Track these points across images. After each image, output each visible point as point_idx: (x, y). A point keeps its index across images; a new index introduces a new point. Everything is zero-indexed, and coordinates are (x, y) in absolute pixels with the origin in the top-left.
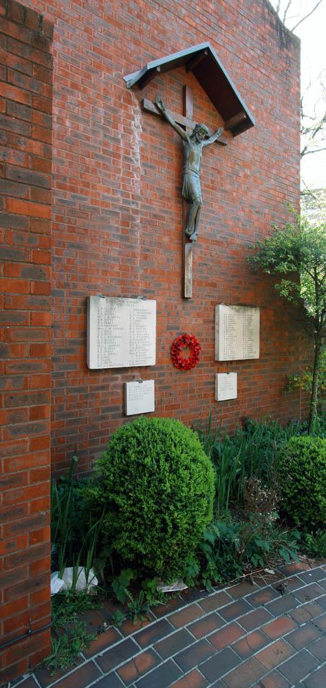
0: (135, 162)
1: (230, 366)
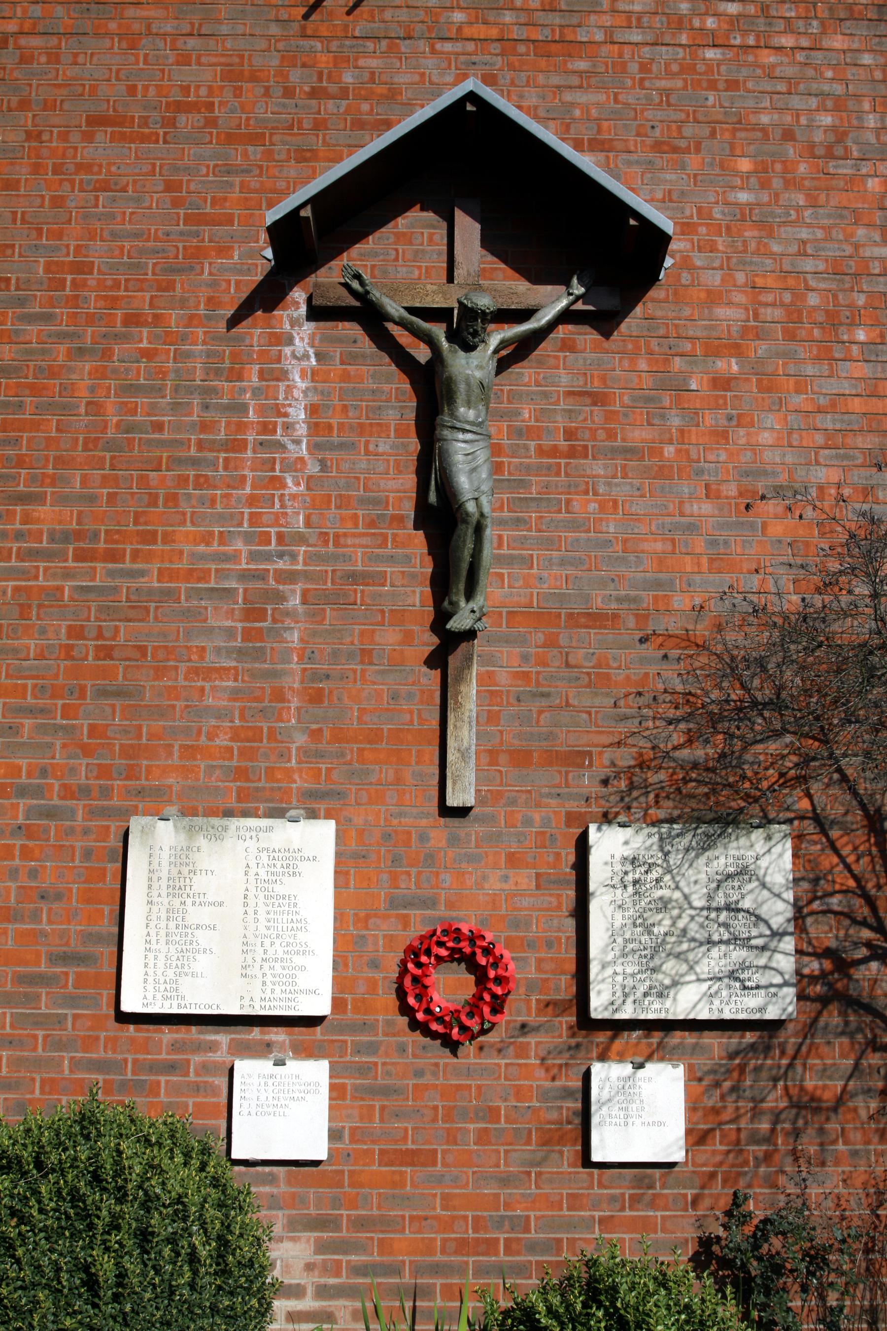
0: (291, 446)
1: (657, 1036)
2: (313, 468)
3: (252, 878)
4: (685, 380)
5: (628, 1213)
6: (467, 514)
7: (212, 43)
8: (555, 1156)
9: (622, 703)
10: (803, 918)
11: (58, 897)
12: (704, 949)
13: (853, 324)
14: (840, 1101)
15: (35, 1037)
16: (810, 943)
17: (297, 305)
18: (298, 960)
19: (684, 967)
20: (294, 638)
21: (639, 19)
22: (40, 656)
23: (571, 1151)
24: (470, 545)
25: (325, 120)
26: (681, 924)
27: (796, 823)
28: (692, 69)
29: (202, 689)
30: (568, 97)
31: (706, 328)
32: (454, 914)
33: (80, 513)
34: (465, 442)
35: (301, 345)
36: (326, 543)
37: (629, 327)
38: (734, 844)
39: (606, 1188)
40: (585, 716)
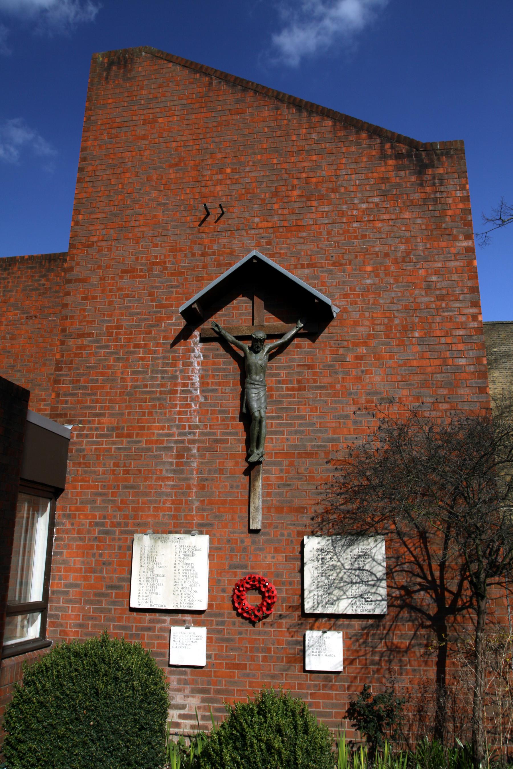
0: (194, 392)
2: (202, 400)
3: (177, 557)
4: (345, 357)
5: (321, 691)
6: (255, 417)
7: (166, 238)
8: (293, 668)
9: (319, 487)
10: (393, 573)
11: (109, 564)
12: (349, 585)
13: (413, 330)
14: (408, 649)
15: (101, 616)
16: (395, 583)
17: (196, 337)
18: (194, 588)
19: (342, 593)
20: (195, 465)
21: (327, 214)
22: (104, 474)
23: (298, 666)
24: (257, 428)
25: (207, 264)
26: (340, 575)
27: (389, 534)
28: (348, 232)
29: (161, 485)
30: (299, 247)
31: (353, 336)
32: (254, 571)
33: (118, 420)
34: (255, 388)
35: (197, 352)
36: (206, 428)
37: (322, 338)
38: (362, 543)
39: (313, 681)
40: (304, 493)
